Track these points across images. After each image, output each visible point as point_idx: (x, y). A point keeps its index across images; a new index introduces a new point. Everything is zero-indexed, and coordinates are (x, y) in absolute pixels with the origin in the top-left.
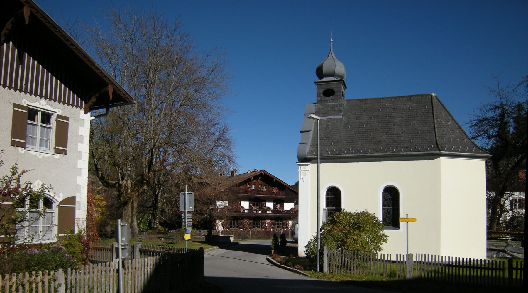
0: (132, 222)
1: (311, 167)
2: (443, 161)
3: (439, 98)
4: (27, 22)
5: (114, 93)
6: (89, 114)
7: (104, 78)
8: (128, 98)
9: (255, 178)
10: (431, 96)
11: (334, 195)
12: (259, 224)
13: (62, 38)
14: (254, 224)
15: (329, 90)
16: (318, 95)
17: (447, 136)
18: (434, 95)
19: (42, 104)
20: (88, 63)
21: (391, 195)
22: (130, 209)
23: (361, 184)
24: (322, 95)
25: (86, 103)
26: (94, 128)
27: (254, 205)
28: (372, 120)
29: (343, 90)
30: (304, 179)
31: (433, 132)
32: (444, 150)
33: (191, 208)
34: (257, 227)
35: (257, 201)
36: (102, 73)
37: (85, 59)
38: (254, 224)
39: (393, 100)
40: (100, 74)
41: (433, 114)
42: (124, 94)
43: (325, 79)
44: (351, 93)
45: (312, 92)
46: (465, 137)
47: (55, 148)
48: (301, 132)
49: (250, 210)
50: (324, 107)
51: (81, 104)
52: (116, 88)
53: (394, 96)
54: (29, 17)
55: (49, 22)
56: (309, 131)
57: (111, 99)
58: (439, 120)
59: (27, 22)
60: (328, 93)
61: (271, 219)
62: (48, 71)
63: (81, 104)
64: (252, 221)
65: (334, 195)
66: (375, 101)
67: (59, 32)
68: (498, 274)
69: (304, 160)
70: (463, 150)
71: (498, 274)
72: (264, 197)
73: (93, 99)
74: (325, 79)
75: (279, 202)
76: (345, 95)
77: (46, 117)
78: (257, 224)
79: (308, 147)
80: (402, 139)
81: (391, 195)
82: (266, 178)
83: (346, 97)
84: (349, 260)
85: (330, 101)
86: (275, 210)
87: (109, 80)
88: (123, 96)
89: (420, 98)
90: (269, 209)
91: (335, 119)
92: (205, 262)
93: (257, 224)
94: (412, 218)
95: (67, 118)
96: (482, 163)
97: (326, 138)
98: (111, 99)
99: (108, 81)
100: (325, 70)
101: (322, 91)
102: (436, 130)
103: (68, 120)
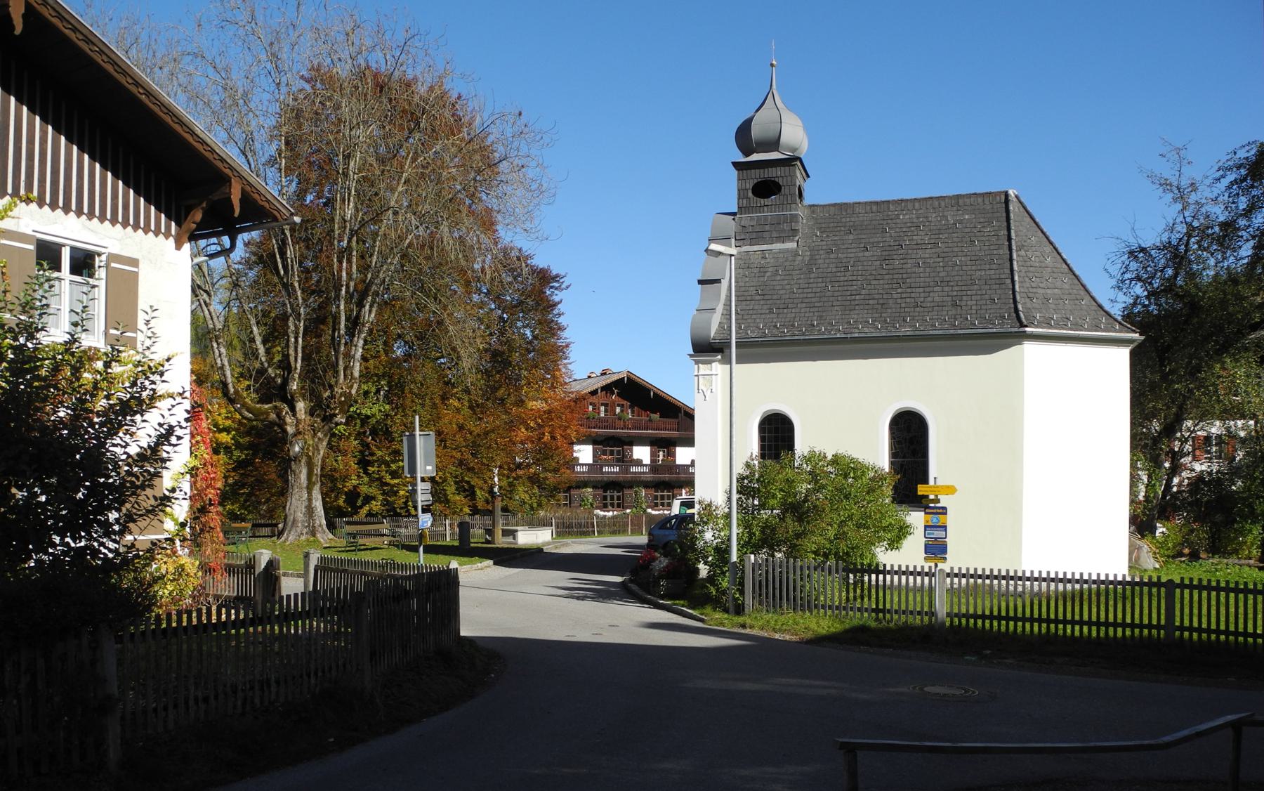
0: (310, 500)
1: (718, 369)
2: (1030, 349)
3: (1022, 200)
4: (18, 30)
5: (246, 199)
6: (187, 247)
7: (219, 164)
8: (279, 211)
9: (607, 388)
10: (1007, 194)
11: (777, 431)
12: (618, 498)
13: (109, 68)
14: (605, 498)
15: (767, 179)
16: (741, 194)
17: (1040, 291)
18: (1011, 192)
19: (70, 230)
20: (177, 127)
21: (909, 433)
22: (304, 471)
23: (842, 408)
24: (750, 194)
25: (179, 224)
26: (1170, 174)
27: (604, 453)
28: (867, 254)
29: (799, 180)
30: (708, 394)
31: (1009, 281)
32: (1031, 324)
33: (429, 468)
34: (612, 505)
35: (613, 444)
36: (213, 151)
37: (168, 119)
38: (605, 498)
39: (917, 205)
40: (207, 154)
41: (1009, 239)
42: (268, 201)
43: (755, 157)
44: (820, 189)
45: (726, 190)
46: (1083, 292)
47: (106, 333)
48: (701, 282)
49: (596, 466)
50: (754, 223)
51: (168, 228)
52: (248, 188)
53: (878, 199)
54: (24, 16)
55: (75, 30)
56: (718, 281)
57: (236, 214)
58: (1023, 253)
59: (18, 30)
60: (766, 189)
61: (647, 485)
62: (82, 149)
63: (168, 228)
64: (600, 492)
65: (777, 431)
66: (874, 208)
67: (101, 52)
68: (1069, 631)
69: (705, 348)
70: (1078, 323)
71: (1069, 631)
72: (629, 436)
73: (198, 216)
74: (755, 157)
75: (665, 445)
76: (805, 194)
77: (84, 263)
78: (612, 498)
79: (716, 319)
80: (937, 299)
81: (909, 433)
82: (631, 390)
83: (808, 199)
84: (799, 583)
85: (770, 209)
86: (654, 467)
87: (231, 168)
88: (267, 205)
89: (980, 200)
90: (639, 463)
91: (781, 251)
92: (463, 592)
93: (612, 498)
94: (948, 487)
95: (134, 262)
96: (1120, 359)
97: (758, 297)
98: (236, 214)
99: (228, 171)
100: (756, 131)
101: (749, 185)
102: (1016, 278)
103: (137, 266)
